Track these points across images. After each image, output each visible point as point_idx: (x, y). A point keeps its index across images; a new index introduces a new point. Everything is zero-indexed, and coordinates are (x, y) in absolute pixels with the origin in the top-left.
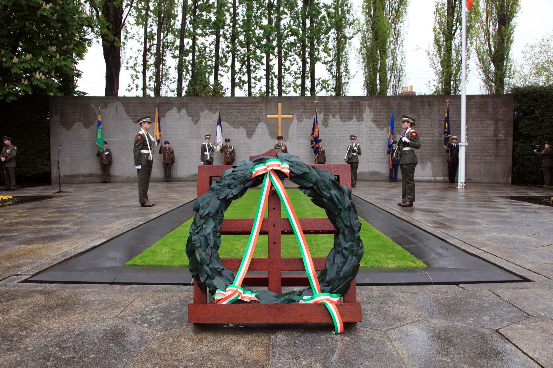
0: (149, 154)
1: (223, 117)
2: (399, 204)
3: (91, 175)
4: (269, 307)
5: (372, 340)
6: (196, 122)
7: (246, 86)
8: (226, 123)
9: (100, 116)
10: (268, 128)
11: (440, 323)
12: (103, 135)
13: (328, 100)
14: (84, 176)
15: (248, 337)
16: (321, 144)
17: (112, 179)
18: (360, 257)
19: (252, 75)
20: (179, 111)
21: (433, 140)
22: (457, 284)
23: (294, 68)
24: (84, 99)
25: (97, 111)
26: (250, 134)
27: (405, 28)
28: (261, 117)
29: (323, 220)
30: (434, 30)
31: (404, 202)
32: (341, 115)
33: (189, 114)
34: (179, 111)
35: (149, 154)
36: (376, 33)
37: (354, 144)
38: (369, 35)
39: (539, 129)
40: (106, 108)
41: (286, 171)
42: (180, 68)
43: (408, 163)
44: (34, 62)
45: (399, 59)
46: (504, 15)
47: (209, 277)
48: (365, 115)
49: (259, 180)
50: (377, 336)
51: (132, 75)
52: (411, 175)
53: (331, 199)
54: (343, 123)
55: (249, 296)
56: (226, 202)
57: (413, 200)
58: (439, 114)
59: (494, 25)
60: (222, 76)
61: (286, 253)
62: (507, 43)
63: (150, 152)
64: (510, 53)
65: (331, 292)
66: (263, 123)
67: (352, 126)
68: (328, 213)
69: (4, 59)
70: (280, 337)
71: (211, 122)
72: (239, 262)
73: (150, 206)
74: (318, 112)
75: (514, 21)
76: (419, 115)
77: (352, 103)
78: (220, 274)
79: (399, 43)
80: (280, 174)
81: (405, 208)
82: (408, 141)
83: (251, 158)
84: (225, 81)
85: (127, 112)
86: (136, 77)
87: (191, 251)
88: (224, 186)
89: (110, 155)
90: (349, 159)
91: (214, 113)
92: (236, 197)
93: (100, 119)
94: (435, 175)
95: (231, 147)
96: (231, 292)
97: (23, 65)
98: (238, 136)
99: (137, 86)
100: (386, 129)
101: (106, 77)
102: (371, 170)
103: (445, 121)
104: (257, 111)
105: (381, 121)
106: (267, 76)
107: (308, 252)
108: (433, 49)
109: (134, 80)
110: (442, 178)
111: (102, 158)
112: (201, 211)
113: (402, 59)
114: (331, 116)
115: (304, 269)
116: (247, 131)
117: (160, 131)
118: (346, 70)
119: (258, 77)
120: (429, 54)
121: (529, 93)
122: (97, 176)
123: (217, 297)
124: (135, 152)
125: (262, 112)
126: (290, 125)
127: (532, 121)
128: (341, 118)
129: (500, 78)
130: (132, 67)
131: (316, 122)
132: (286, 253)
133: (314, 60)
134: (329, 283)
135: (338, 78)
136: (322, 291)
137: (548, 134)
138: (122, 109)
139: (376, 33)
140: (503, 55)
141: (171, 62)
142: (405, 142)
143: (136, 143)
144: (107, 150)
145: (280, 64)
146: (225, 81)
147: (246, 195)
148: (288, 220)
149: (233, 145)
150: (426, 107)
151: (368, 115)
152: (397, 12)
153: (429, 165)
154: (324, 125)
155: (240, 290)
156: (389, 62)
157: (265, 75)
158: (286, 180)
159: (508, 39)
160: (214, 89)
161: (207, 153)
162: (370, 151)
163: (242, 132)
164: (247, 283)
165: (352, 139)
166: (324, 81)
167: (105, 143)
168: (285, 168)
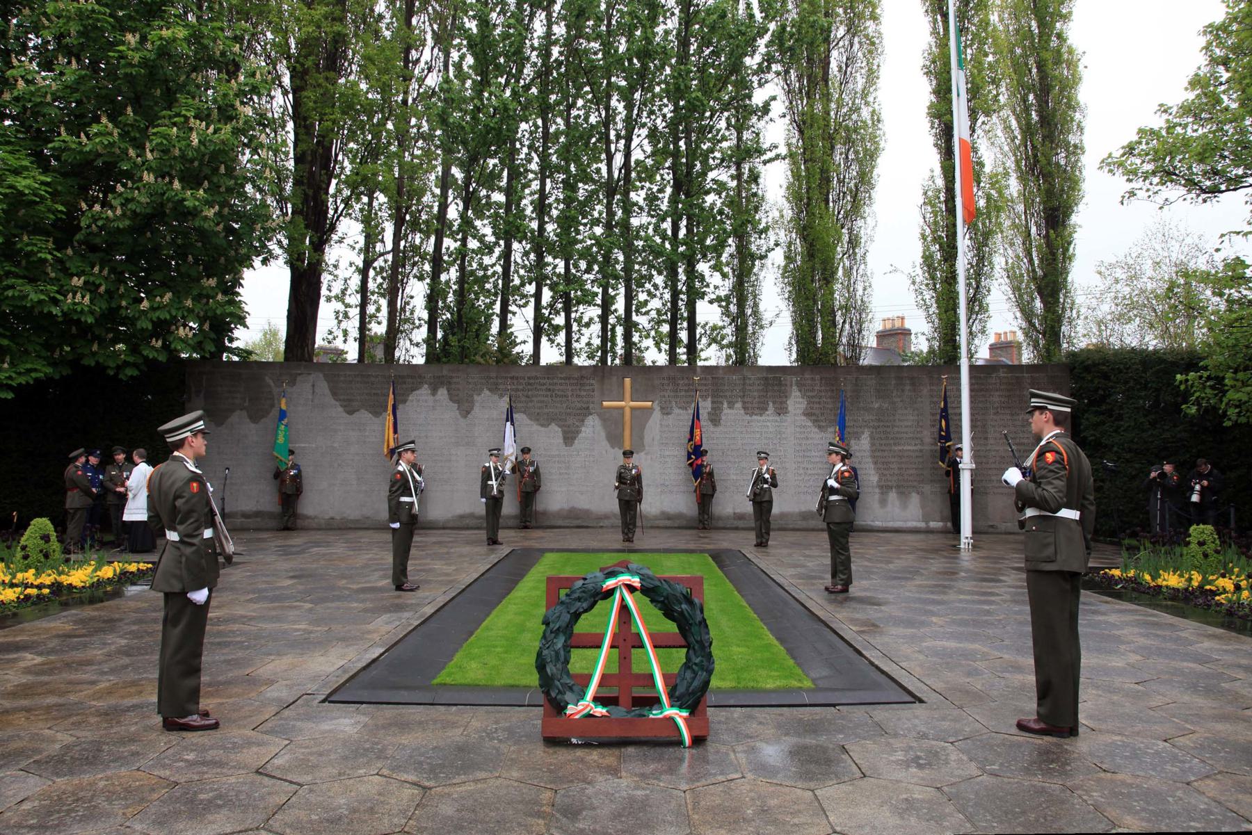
0: (413, 503)
1: (519, 405)
2: (827, 589)
3: (258, 514)
4: (620, 722)
5: (718, 752)
6: (466, 413)
7: (561, 338)
8: (524, 416)
9: (283, 401)
10: (605, 427)
11: (791, 740)
12: (288, 439)
13: (720, 374)
14: (245, 515)
15: (599, 750)
16: (706, 459)
17: (300, 523)
18: (710, 672)
19: (573, 315)
20: (434, 391)
21: (921, 451)
22: (834, 705)
23: (655, 304)
24: (248, 362)
25: (276, 390)
26: (569, 437)
27: (868, 231)
28: (591, 406)
29: (674, 634)
30: (924, 237)
31: (834, 584)
32: (744, 403)
33: (453, 398)
34: (434, 391)
35: (413, 503)
36: (811, 245)
37: (765, 468)
38: (798, 246)
39: (1116, 431)
40: (294, 384)
41: (637, 585)
42: (432, 300)
43: (837, 521)
44: (176, 306)
45: (860, 288)
46: (1055, 209)
47: (560, 692)
48: (791, 404)
49: (610, 593)
50: (723, 749)
51: (337, 313)
52: (842, 540)
53: (682, 613)
54: (748, 417)
55: (600, 711)
56: (576, 616)
57: (847, 583)
58: (932, 402)
59: (1038, 226)
60: (514, 314)
61: (636, 669)
62: (1064, 261)
63: (414, 499)
64: (1069, 279)
65: (681, 707)
66: (596, 417)
67: (767, 422)
68: (679, 627)
69: (124, 303)
70: (631, 750)
71: (495, 414)
72: (589, 678)
73: (412, 590)
74: (701, 397)
75: (1074, 219)
76: (894, 403)
77: (766, 379)
78: (571, 689)
79: (858, 257)
80: (631, 589)
81: (833, 596)
82: (836, 485)
83: (602, 570)
84: (522, 323)
85: (334, 394)
86: (346, 316)
87: (541, 666)
88: (575, 600)
89: (298, 476)
90: (755, 494)
91: (501, 396)
92: (586, 611)
93: (284, 407)
94: (926, 519)
95: (532, 463)
96: (584, 706)
97: (157, 313)
98: (547, 442)
99: (345, 333)
100: (831, 430)
101: (288, 317)
102: (803, 509)
103: (942, 417)
104: (583, 393)
105: (822, 414)
106: (604, 319)
107: (656, 666)
108: (920, 274)
109: (340, 322)
110: (941, 524)
111: (283, 481)
112: (551, 625)
113: (865, 289)
114: (725, 405)
115: (653, 685)
116: (564, 432)
117: (395, 432)
118: (756, 313)
119: (586, 319)
120: (914, 283)
121: (1095, 365)
122: (270, 515)
123: (568, 712)
124: (390, 501)
125: (593, 397)
126: (647, 421)
127: (1102, 417)
128: (745, 408)
129: (1053, 327)
130: (337, 297)
131: (696, 416)
132: (636, 669)
133: (694, 295)
134: (679, 699)
135: (741, 330)
136: (672, 706)
137: (1132, 441)
138: (323, 387)
139: (811, 245)
140: (1055, 283)
141: (417, 291)
142: (832, 487)
143: (392, 486)
144: (293, 467)
145: (629, 298)
146: (522, 323)
147: (597, 606)
148: (638, 635)
149: (536, 459)
150: (908, 388)
151: (796, 402)
152: (855, 197)
153: (915, 499)
154: (712, 421)
155: (592, 705)
156: (839, 298)
157: (599, 316)
158: (638, 593)
159: (1064, 254)
160: (500, 349)
161: (493, 483)
162: (801, 471)
163: (555, 431)
164: (597, 700)
165: (760, 459)
166: (714, 328)
167: (292, 452)
168: (636, 581)
